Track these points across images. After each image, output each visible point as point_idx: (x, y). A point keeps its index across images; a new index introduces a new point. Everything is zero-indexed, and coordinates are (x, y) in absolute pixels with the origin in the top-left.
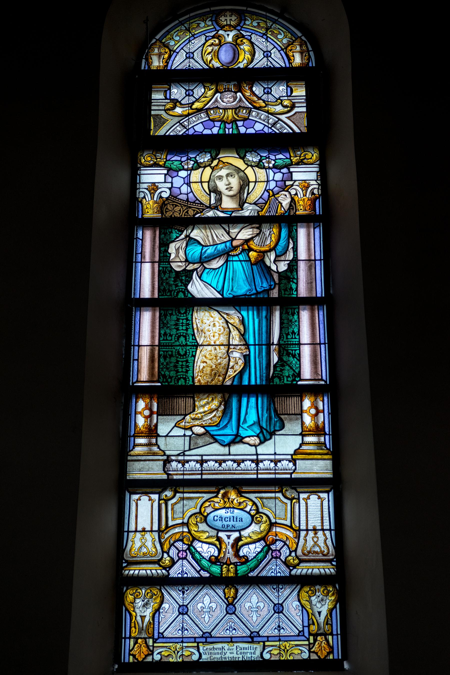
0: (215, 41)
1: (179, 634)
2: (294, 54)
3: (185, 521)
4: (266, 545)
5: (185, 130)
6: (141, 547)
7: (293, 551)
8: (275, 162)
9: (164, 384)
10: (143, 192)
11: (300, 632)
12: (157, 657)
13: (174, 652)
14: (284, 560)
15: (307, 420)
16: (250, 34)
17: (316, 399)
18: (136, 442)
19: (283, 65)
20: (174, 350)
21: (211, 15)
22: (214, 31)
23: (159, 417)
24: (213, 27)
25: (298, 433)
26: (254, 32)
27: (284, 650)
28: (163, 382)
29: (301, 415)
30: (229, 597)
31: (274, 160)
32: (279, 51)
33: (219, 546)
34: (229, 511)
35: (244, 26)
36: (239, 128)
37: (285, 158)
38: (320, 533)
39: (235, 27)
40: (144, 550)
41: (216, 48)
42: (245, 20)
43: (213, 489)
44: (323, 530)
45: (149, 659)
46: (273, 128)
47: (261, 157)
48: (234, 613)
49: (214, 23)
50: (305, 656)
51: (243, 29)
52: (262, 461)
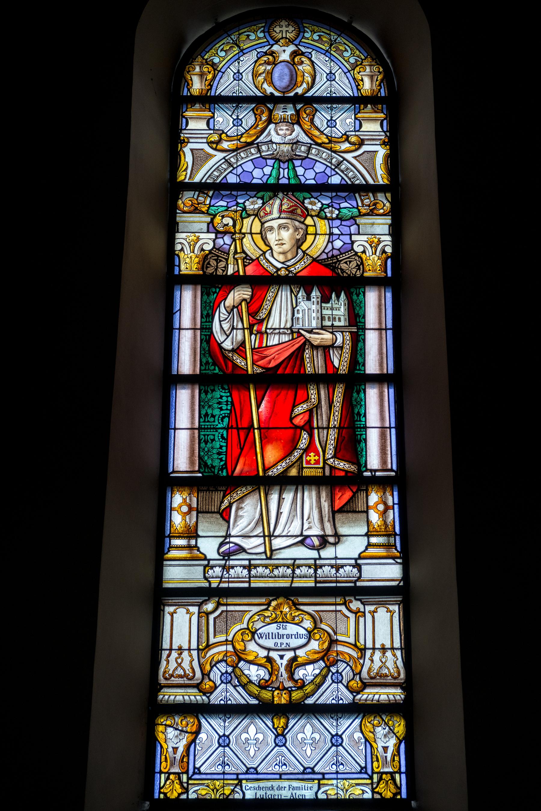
0: (269, 59)
1: (220, 769)
2: (363, 77)
3: (230, 638)
4: (326, 666)
5: (232, 168)
6: (176, 669)
7: (357, 674)
8: (340, 212)
9: (205, 474)
10: (180, 243)
11: (362, 768)
12: (192, 796)
13: (213, 790)
14: (345, 684)
15: (374, 517)
16: (311, 50)
17: (384, 493)
18: (172, 544)
19: (352, 95)
20: (217, 434)
21: (263, 25)
22: (267, 46)
23: (200, 515)
24: (265, 40)
25: (364, 534)
26: (314, 48)
27: (342, 790)
28: (205, 472)
29: (367, 512)
30: (278, 727)
31: (338, 210)
32: (345, 73)
33: (270, 669)
34: (281, 626)
35: (303, 40)
36: (296, 168)
37: (351, 206)
38: (389, 654)
39: (291, 42)
40: (180, 672)
41: (269, 67)
42: (304, 32)
43: (263, 600)
44: (392, 649)
45: (184, 796)
46: (336, 170)
47: (323, 204)
48: (284, 745)
49: (267, 34)
50: (368, 795)
51: (301, 44)
52: (321, 567)
